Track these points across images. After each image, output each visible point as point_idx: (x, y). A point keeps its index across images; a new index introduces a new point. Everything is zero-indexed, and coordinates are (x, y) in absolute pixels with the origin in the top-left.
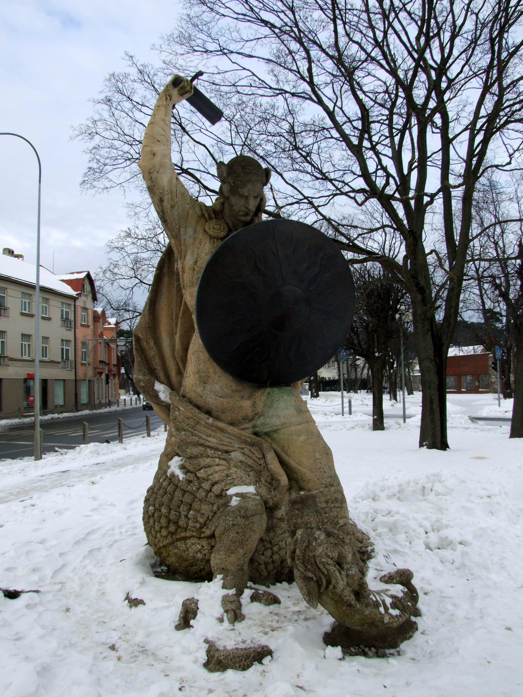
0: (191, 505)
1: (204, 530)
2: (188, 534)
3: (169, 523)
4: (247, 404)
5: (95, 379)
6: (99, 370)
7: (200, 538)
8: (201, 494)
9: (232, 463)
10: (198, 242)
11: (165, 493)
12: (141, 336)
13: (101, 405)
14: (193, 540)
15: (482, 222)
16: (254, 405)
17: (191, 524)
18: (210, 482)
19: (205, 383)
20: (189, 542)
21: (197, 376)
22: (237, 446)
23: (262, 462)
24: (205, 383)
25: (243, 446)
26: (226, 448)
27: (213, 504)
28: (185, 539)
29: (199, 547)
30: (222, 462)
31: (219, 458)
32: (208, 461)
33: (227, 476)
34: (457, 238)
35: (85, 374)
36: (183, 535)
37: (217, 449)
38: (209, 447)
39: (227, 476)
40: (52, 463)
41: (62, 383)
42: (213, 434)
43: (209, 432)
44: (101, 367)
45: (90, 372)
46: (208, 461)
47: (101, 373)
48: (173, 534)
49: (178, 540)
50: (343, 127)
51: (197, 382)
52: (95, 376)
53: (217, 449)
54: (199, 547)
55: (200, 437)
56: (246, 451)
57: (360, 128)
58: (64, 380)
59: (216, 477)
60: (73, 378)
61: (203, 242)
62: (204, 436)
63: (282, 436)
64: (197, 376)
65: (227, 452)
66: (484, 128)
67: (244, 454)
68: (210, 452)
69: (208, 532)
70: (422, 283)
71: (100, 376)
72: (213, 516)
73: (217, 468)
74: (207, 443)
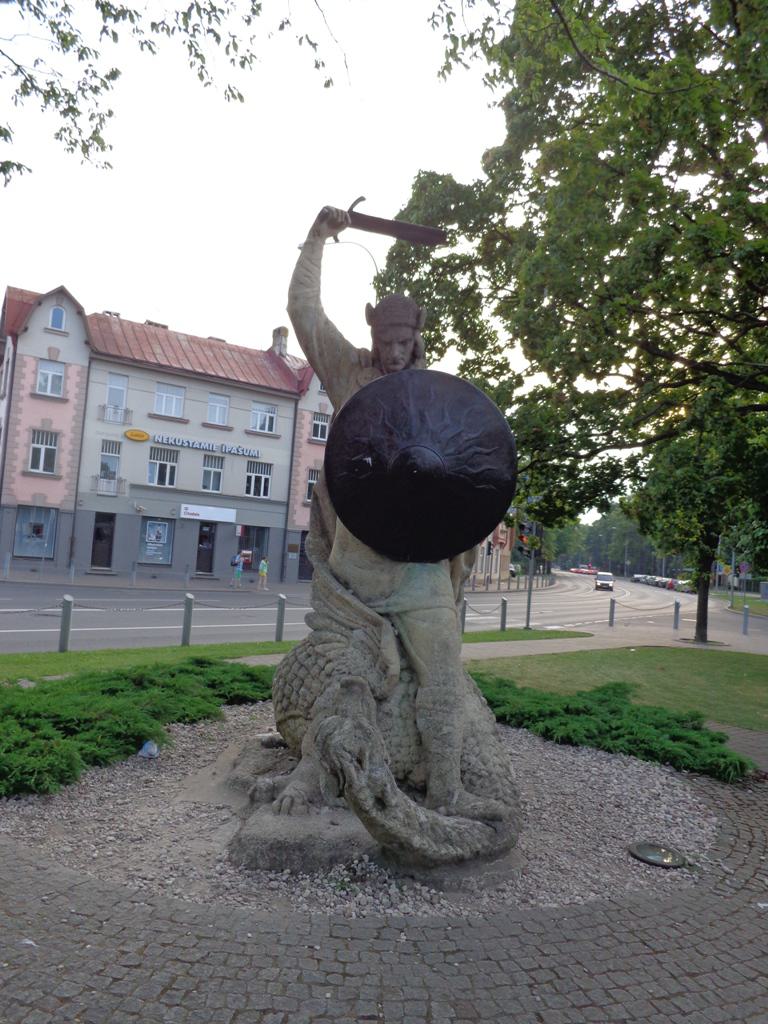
4: (385, 577)
8: (315, 670)
16: (392, 581)
18: (325, 659)
22: (361, 623)
26: (351, 624)
30: (343, 639)
31: (342, 635)
32: (330, 635)
33: (343, 655)
37: (343, 625)
38: (336, 621)
39: (343, 655)
53: (343, 625)
55: (331, 609)
56: (368, 630)
59: (331, 654)
62: (335, 609)
68: (335, 626)
74: (335, 617)
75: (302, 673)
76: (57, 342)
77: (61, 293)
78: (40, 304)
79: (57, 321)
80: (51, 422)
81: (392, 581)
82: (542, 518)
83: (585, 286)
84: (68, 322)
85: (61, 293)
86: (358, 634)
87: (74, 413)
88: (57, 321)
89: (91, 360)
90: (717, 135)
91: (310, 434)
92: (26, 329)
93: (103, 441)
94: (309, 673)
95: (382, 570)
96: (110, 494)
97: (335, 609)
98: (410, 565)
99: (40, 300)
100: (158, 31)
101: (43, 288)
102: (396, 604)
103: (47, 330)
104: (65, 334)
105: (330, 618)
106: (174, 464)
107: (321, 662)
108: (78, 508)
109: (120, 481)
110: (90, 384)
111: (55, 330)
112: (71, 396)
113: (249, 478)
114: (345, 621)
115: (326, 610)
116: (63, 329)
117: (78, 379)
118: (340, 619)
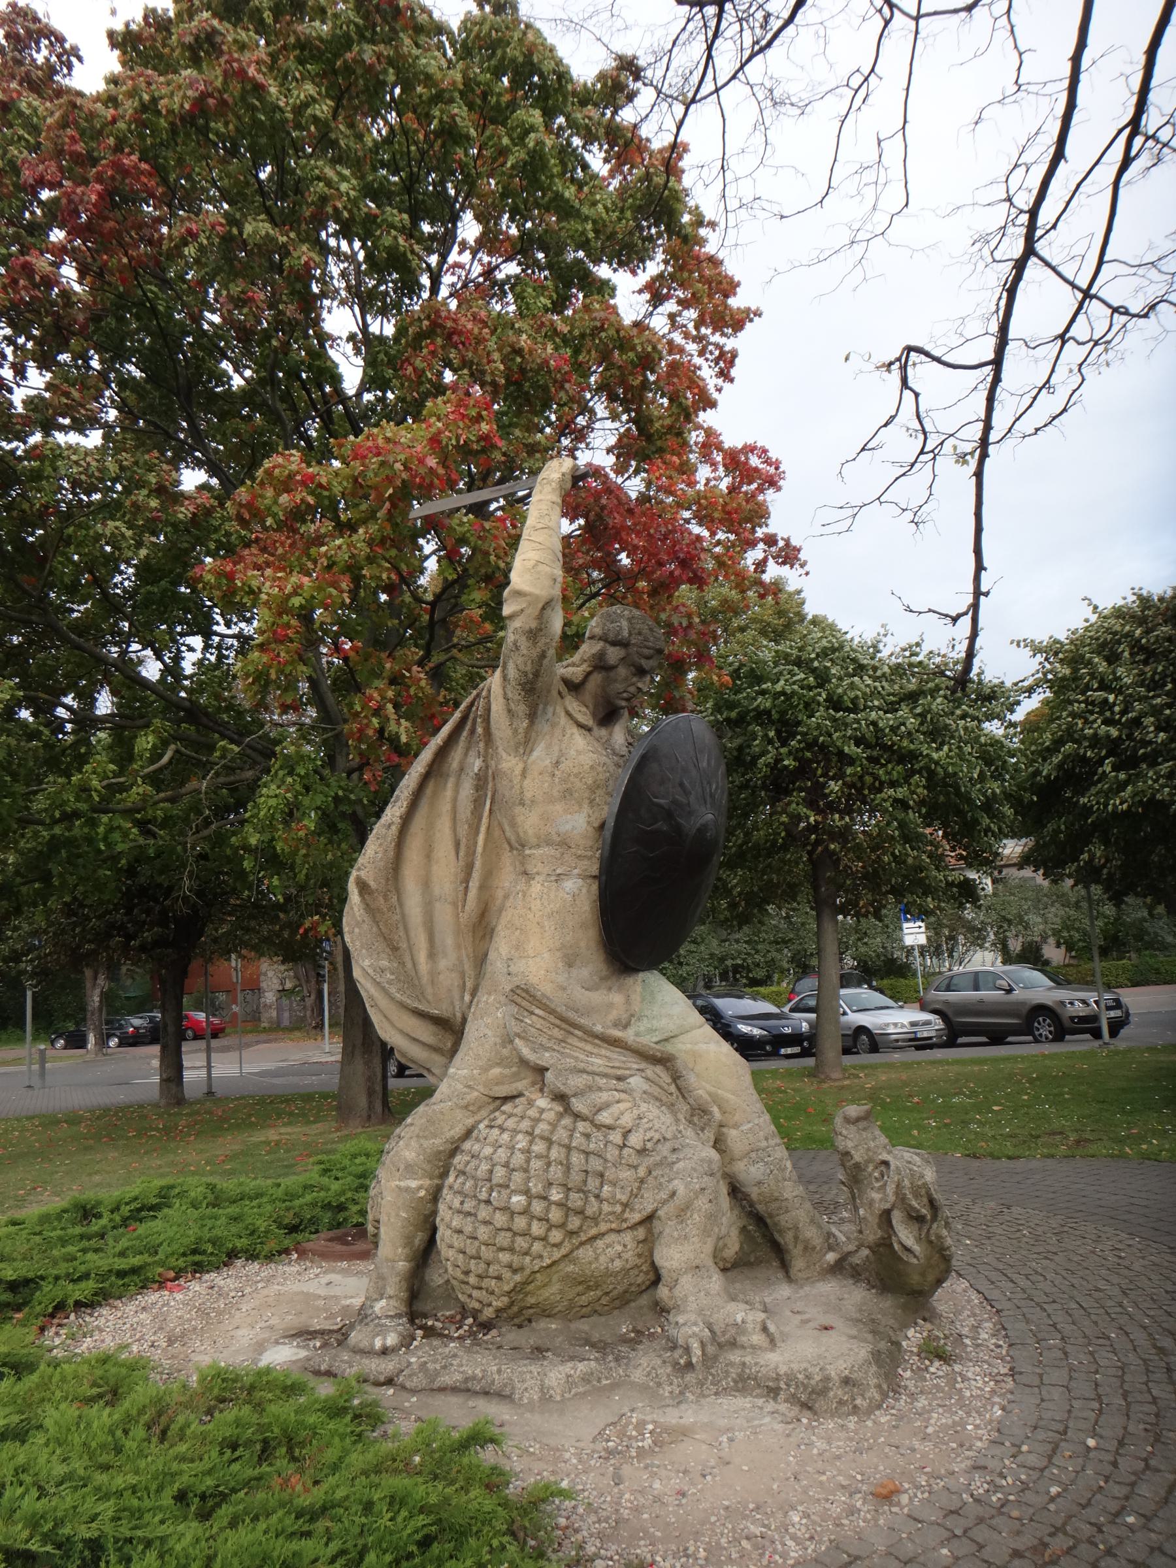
0: (602, 1175)
1: (626, 1215)
2: (603, 1227)
3: (567, 1216)
4: (617, 998)
7: (619, 1231)
9: (637, 1095)
10: (558, 732)
11: (549, 1164)
12: (372, 884)
14: (609, 1239)
17: (606, 1207)
19: (570, 966)
20: (600, 1243)
21: (558, 954)
22: (635, 1066)
23: (673, 1089)
24: (570, 966)
25: (643, 1065)
26: (619, 1072)
27: (635, 1167)
28: (594, 1238)
29: (619, 1248)
30: (623, 1096)
32: (605, 1096)
36: (593, 1232)
37: (605, 1075)
40: (273, 1045)
42: (595, 1051)
43: (589, 1047)
48: (572, 1233)
49: (582, 1244)
51: (560, 965)
53: (605, 1075)
54: (619, 1248)
55: (576, 1059)
56: (649, 1073)
59: (627, 1120)
61: (569, 732)
62: (582, 1057)
63: (680, 1046)
64: (558, 954)
65: (620, 1079)
67: (647, 1079)
69: (636, 1217)
72: (639, 1188)
73: (622, 1106)
74: (590, 1068)
75: (595, 1164)
81: (628, 1001)
82: (776, 977)
83: (507, 107)
86: (635, 1082)
90: (75, 925)
91: (21, 1040)
94: (606, 1160)
95: (610, 989)
97: (582, 1057)
98: (641, 975)
100: (787, 542)
102: (651, 1031)
105: (584, 1071)
107: (616, 1137)
114: (609, 1071)
115: (570, 1062)
118: (595, 1069)
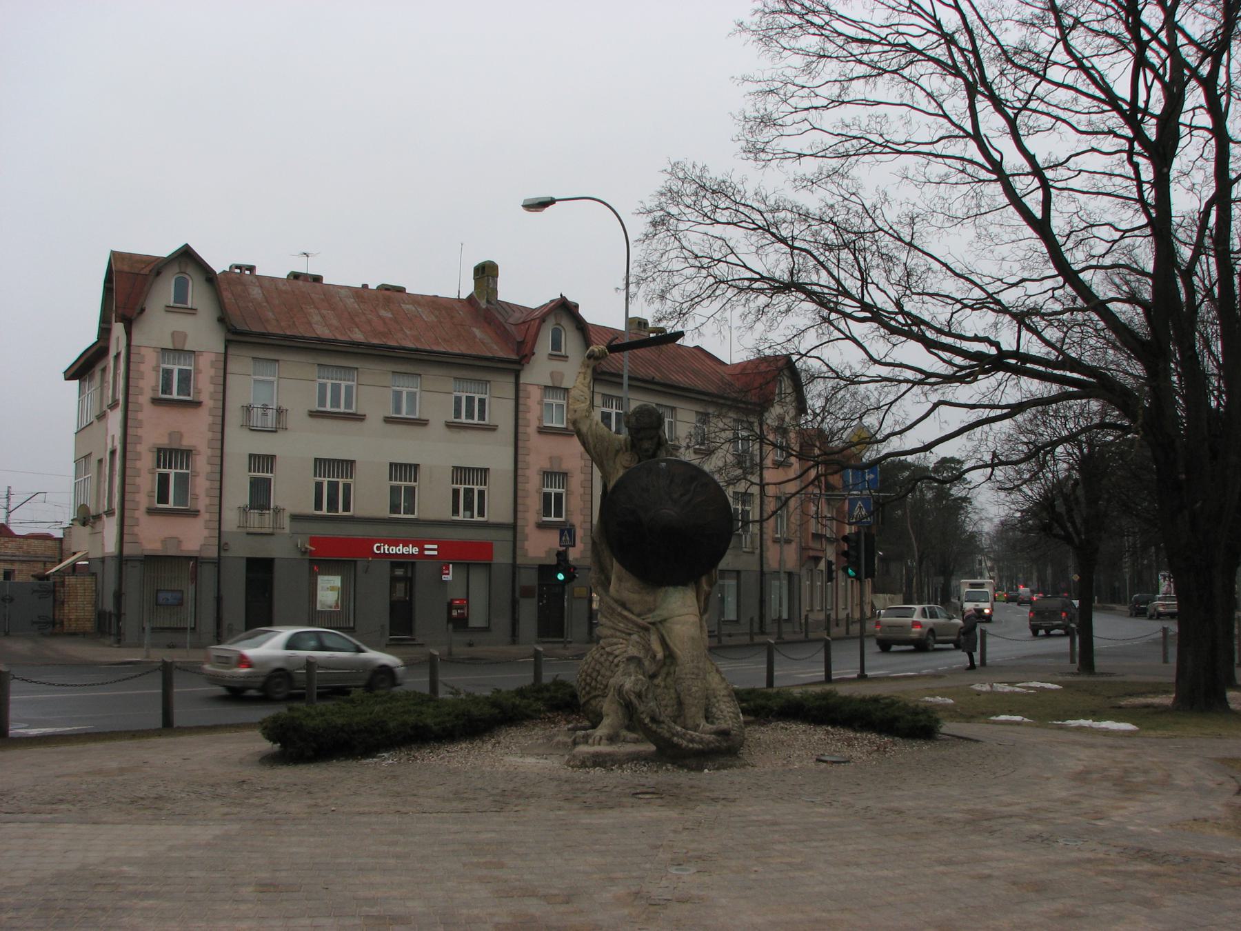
5: (804, 572)
6: (812, 553)
13: (141, 669)
15: (1107, 90)
32: (615, 640)
34: (1103, 97)
35: (781, 562)
41: (734, 575)
44: (818, 546)
45: (791, 556)
46: (615, 640)
47: (817, 559)
50: (1021, 351)
52: (802, 565)
57: (1081, 275)
58: (738, 572)
60: (756, 568)
66: (1224, 99)
68: (618, 634)
70: (519, 465)
71: (817, 565)
76: (558, 366)
77: (186, 255)
78: (158, 273)
79: (181, 295)
80: (181, 435)
84: (197, 295)
85: (186, 255)
87: (210, 419)
88: (181, 295)
89: (228, 343)
92: (143, 310)
93: (391, 465)
96: (263, 531)
99: (152, 269)
101: (164, 248)
103: (169, 309)
104: (192, 311)
106: (348, 480)
108: (223, 554)
109: (277, 511)
110: (229, 377)
111: (180, 306)
112: (205, 397)
113: (456, 492)
116: (563, 353)
117: (212, 372)
